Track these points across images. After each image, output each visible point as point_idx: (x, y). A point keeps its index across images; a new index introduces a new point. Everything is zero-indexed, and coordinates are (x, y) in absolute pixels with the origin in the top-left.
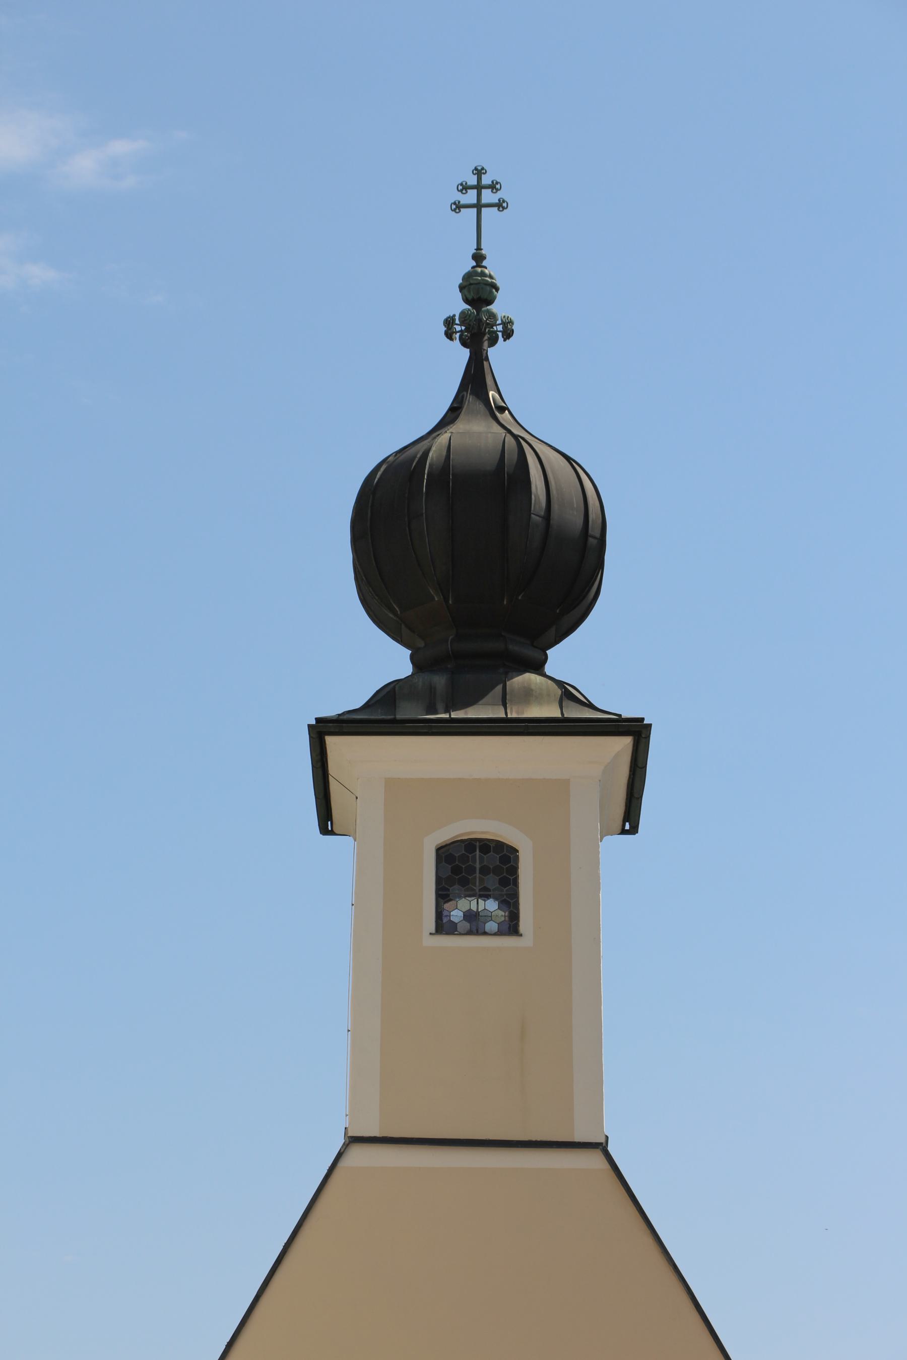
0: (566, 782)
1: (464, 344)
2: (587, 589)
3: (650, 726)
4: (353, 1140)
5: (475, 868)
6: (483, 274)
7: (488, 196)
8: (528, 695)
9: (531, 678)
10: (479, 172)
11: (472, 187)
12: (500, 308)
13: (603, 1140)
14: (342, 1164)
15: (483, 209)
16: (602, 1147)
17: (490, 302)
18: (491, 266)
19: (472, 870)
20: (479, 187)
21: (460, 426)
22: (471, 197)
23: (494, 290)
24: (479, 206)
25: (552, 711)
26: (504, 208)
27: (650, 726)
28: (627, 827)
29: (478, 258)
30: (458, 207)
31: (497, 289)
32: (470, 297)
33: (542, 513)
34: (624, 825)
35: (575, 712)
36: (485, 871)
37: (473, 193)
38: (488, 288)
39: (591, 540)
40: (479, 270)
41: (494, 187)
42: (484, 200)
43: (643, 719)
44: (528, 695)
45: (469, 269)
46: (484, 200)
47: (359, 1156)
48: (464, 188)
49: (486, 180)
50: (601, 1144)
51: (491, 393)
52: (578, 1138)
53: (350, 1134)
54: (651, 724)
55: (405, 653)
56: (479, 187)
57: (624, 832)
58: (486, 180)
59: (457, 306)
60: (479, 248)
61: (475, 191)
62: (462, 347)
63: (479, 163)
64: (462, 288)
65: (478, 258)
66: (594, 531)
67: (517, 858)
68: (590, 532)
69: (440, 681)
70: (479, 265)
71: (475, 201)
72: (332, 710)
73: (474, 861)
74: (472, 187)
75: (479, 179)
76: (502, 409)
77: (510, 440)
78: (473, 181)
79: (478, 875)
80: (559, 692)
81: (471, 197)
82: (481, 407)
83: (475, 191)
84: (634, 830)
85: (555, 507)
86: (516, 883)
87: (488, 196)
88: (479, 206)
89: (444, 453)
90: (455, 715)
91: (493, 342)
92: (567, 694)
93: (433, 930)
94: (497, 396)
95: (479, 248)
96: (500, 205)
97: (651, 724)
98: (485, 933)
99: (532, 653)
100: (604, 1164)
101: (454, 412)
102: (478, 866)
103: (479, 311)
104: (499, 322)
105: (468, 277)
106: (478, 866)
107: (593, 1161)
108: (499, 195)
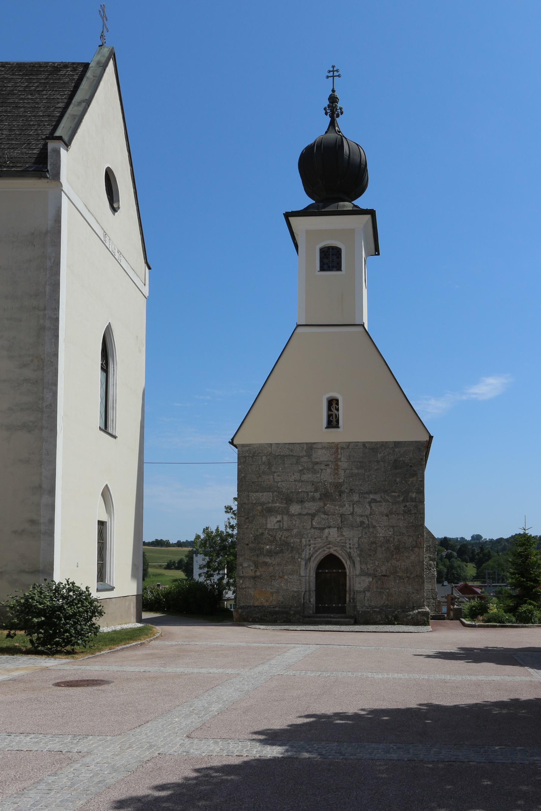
2: (255, 645)
4: (298, 326)
6: (334, 95)
10: (333, 67)
11: (331, 71)
12: (339, 105)
13: (363, 324)
14: (295, 332)
15: (335, 77)
16: (363, 325)
18: (337, 94)
20: (333, 71)
22: (331, 74)
24: (333, 76)
28: (377, 253)
29: (333, 91)
30: (328, 77)
33: (348, 155)
35: (104, 242)
36: (333, 255)
37: (332, 73)
38: (335, 98)
39: (362, 165)
41: (337, 71)
42: (335, 75)
46: (335, 75)
47: (300, 330)
48: (330, 72)
49: (335, 69)
50: (362, 324)
51: (336, 128)
52: (356, 323)
53: (298, 324)
56: (333, 71)
57: (376, 255)
58: (335, 69)
60: (333, 88)
61: (332, 72)
64: (329, 99)
65: (333, 91)
66: (363, 166)
67: (341, 251)
69: (321, 204)
74: (331, 71)
75: (333, 69)
78: (332, 69)
80: (353, 205)
82: (334, 131)
83: (332, 72)
84: (379, 254)
85: (351, 154)
88: (333, 76)
94: (338, 129)
95: (333, 88)
96: (339, 76)
100: (363, 330)
102: (331, 253)
105: (331, 95)
106: (331, 253)
107: (360, 329)
108: (339, 73)
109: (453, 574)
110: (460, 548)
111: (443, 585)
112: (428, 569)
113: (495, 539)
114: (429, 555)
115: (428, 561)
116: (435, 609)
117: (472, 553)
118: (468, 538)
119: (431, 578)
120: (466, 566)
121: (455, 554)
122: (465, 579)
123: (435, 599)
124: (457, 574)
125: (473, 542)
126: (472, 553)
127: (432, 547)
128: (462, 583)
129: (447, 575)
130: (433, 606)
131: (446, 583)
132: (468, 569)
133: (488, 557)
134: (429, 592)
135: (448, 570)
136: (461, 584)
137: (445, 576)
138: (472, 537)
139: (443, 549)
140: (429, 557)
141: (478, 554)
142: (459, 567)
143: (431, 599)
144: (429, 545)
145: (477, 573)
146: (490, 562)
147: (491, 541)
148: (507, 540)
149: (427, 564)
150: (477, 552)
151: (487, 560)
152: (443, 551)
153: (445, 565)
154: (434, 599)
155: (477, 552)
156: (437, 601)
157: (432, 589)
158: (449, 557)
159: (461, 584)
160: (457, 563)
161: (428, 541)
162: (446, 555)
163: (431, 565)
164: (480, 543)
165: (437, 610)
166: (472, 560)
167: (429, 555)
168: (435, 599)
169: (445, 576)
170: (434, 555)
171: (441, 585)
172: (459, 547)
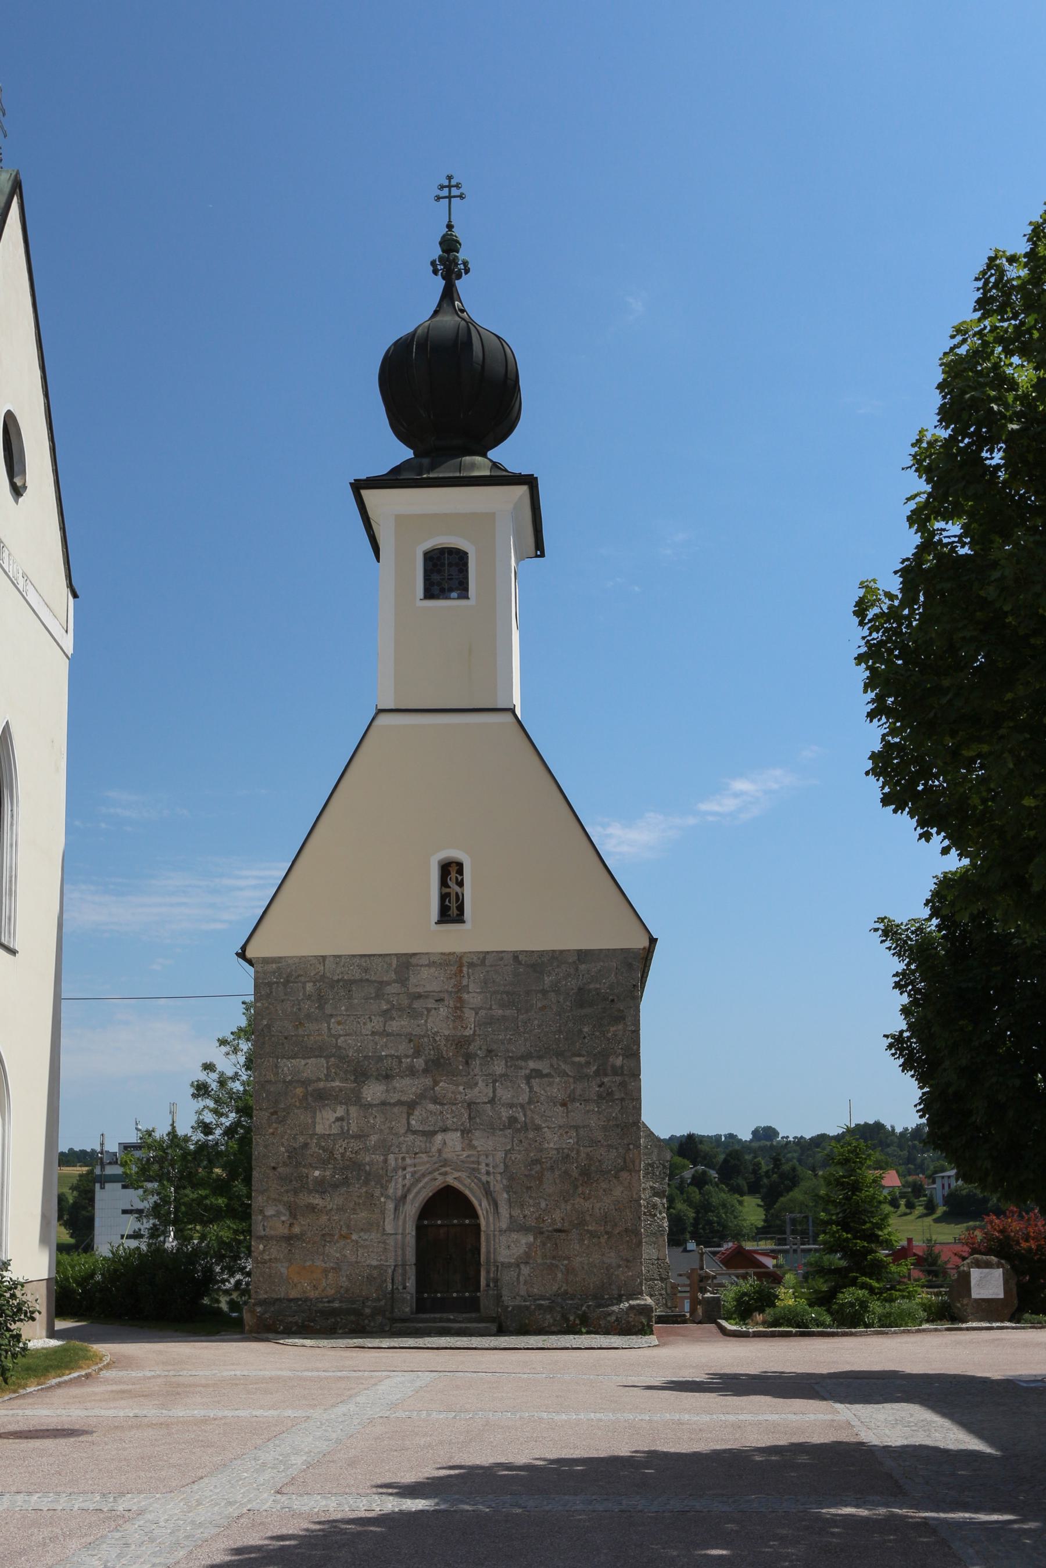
1: (444, 278)
3: (537, 478)
5: (445, 564)
6: (451, 235)
7: (455, 192)
8: (473, 466)
9: (478, 459)
10: (450, 178)
11: (446, 187)
12: (462, 255)
13: (512, 707)
14: (374, 724)
16: (512, 711)
18: (457, 232)
19: (443, 565)
20: (449, 187)
21: (437, 318)
22: (445, 192)
24: (450, 197)
26: (464, 198)
27: (537, 478)
28: (539, 553)
29: (450, 227)
30: (438, 198)
31: (460, 244)
32: (445, 248)
34: (536, 553)
36: (450, 565)
38: (454, 243)
40: (449, 233)
41: (457, 186)
43: (533, 475)
44: (473, 466)
45: (445, 232)
47: (383, 720)
48: (442, 187)
51: (456, 303)
53: (379, 708)
55: (412, 451)
56: (449, 187)
57: (537, 556)
58: (453, 182)
59: (437, 252)
62: (777, 1129)
63: (449, 173)
64: (441, 243)
65: (450, 227)
68: (509, 376)
69: (426, 461)
70: (450, 230)
71: (447, 195)
73: (444, 559)
74: (446, 187)
76: (463, 311)
77: (463, 323)
78: (446, 183)
79: (446, 567)
80: (491, 464)
81: (445, 192)
84: (542, 555)
86: (467, 571)
87: (455, 192)
88: (450, 197)
89: (426, 330)
90: (431, 475)
91: (459, 277)
92: (495, 465)
93: (422, 597)
96: (461, 197)
98: (450, 599)
101: (436, 313)
103: (448, 255)
104: (460, 262)
105: (444, 236)
107: (508, 718)
108: (461, 190)
109: (710, 1223)
110: (726, 1161)
111: (685, 1250)
112: (651, 1215)
113: (808, 1136)
114: (651, 1184)
115: (650, 1197)
116: (666, 1302)
117: (755, 1172)
118: (746, 1136)
119: (655, 1233)
120: (741, 1203)
121: (714, 1174)
122: (738, 1236)
123: (666, 1279)
124: (719, 1223)
125: (755, 1145)
126: (755, 1172)
127: (657, 1167)
128: (730, 1244)
129: (696, 1224)
130: (661, 1295)
131: (691, 1245)
132: (745, 1210)
133: (792, 1180)
134: (653, 1264)
135: (697, 1212)
136: (728, 1246)
137: (690, 1229)
138: (755, 1133)
139: (686, 1162)
140: (651, 1187)
141: (767, 1174)
142: (724, 1206)
143: (657, 1280)
144: (650, 1162)
145: (765, 1221)
146: (797, 1194)
147: (800, 1141)
148: (838, 1138)
149: (648, 1203)
150: (764, 1168)
151: (789, 1189)
152: (684, 1167)
153: (689, 1201)
154: (662, 1280)
155: (764, 1168)
156: (669, 1285)
157: (658, 1259)
158: (700, 1181)
159: (728, 1246)
160: (720, 1195)
161: (650, 1154)
162: (694, 1177)
163: (656, 1205)
164: (772, 1147)
165: (669, 1304)
166: (753, 1189)
167: (651, 1184)
168: (666, 1279)
169: (690, 1229)
170: (661, 1184)
171: (681, 1249)
172: (722, 1157)
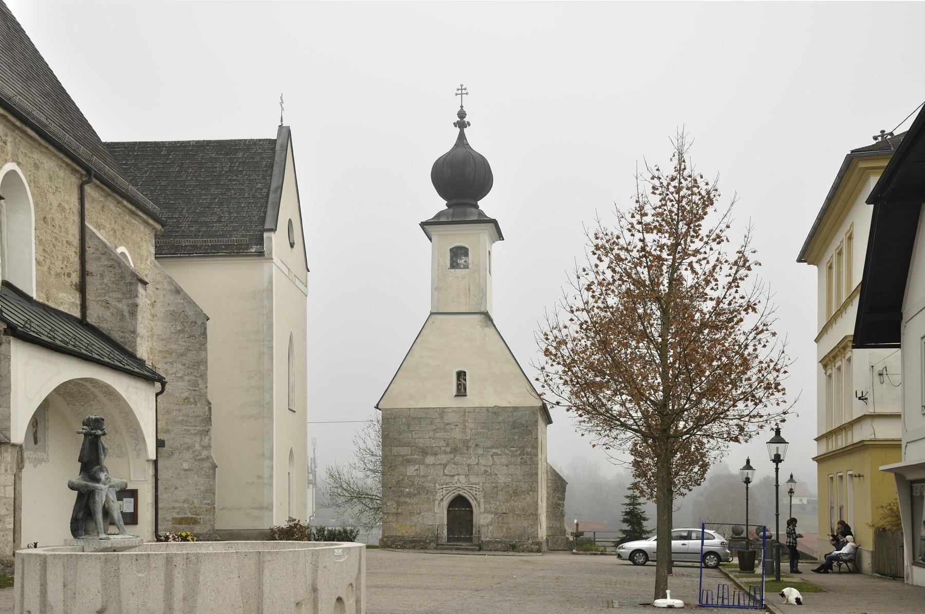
0: (468, 256)
7: (464, 92)
10: (462, 86)
17: (465, 118)
22: (460, 92)
23: (582, 537)
24: (462, 94)
25: (475, 218)
29: (462, 107)
30: (457, 94)
37: (460, 91)
44: (471, 214)
48: (458, 90)
54: (137, 490)
56: (462, 89)
65: (462, 107)
72: (424, 220)
78: (460, 88)
81: (460, 92)
88: (462, 94)
91: (466, 127)
96: (467, 94)
97: (137, 490)
99: (473, 202)
